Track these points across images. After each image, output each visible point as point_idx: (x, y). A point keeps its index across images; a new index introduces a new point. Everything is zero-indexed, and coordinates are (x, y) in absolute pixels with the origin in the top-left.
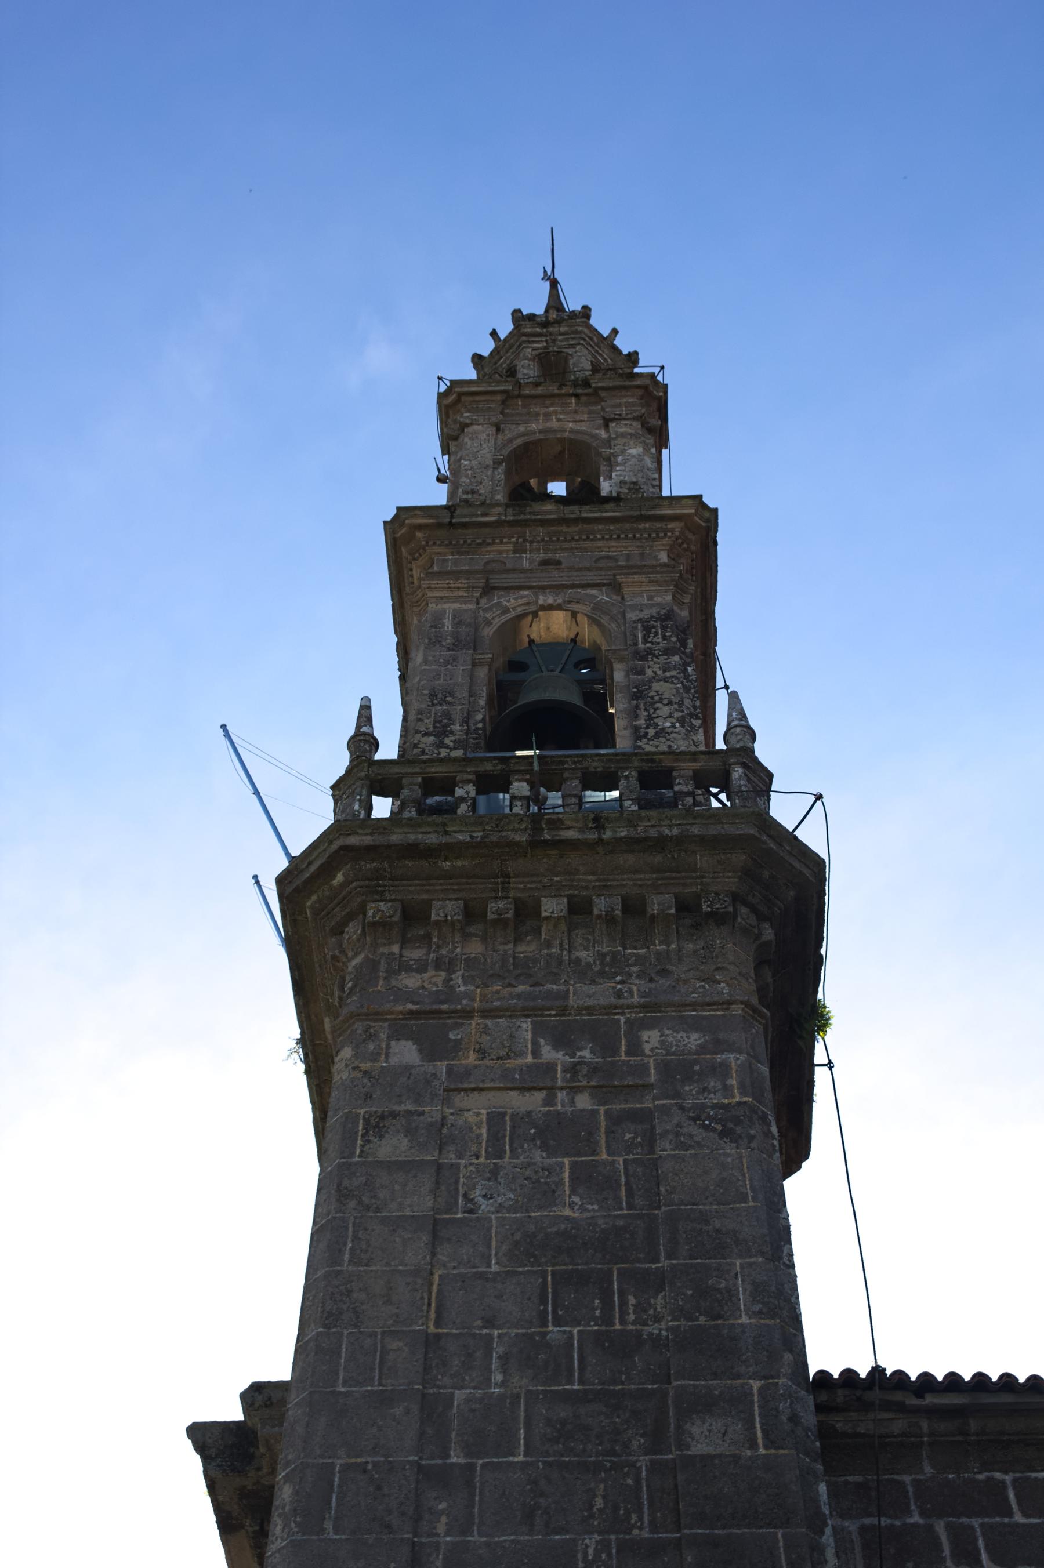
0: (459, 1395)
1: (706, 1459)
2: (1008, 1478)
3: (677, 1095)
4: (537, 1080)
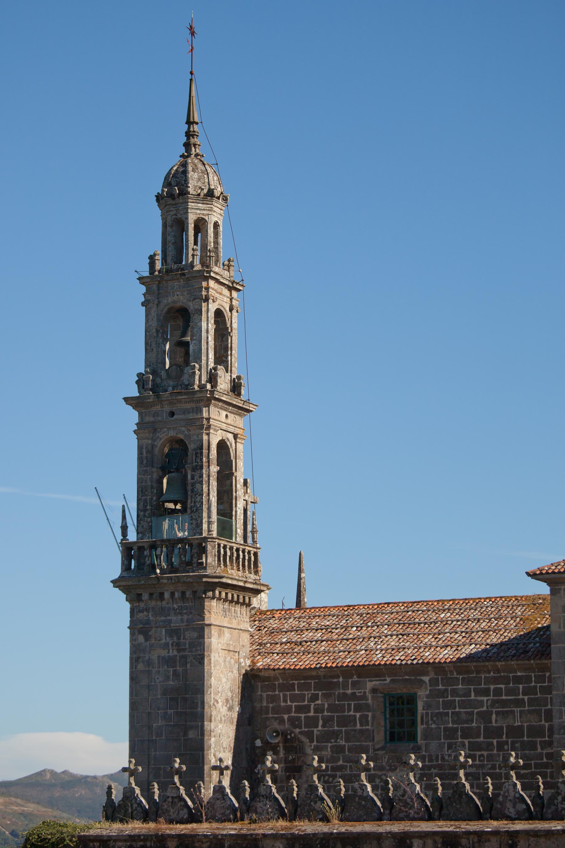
0: (154, 725)
1: (191, 739)
2: (320, 693)
3: (191, 651)
4: (166, 646)
